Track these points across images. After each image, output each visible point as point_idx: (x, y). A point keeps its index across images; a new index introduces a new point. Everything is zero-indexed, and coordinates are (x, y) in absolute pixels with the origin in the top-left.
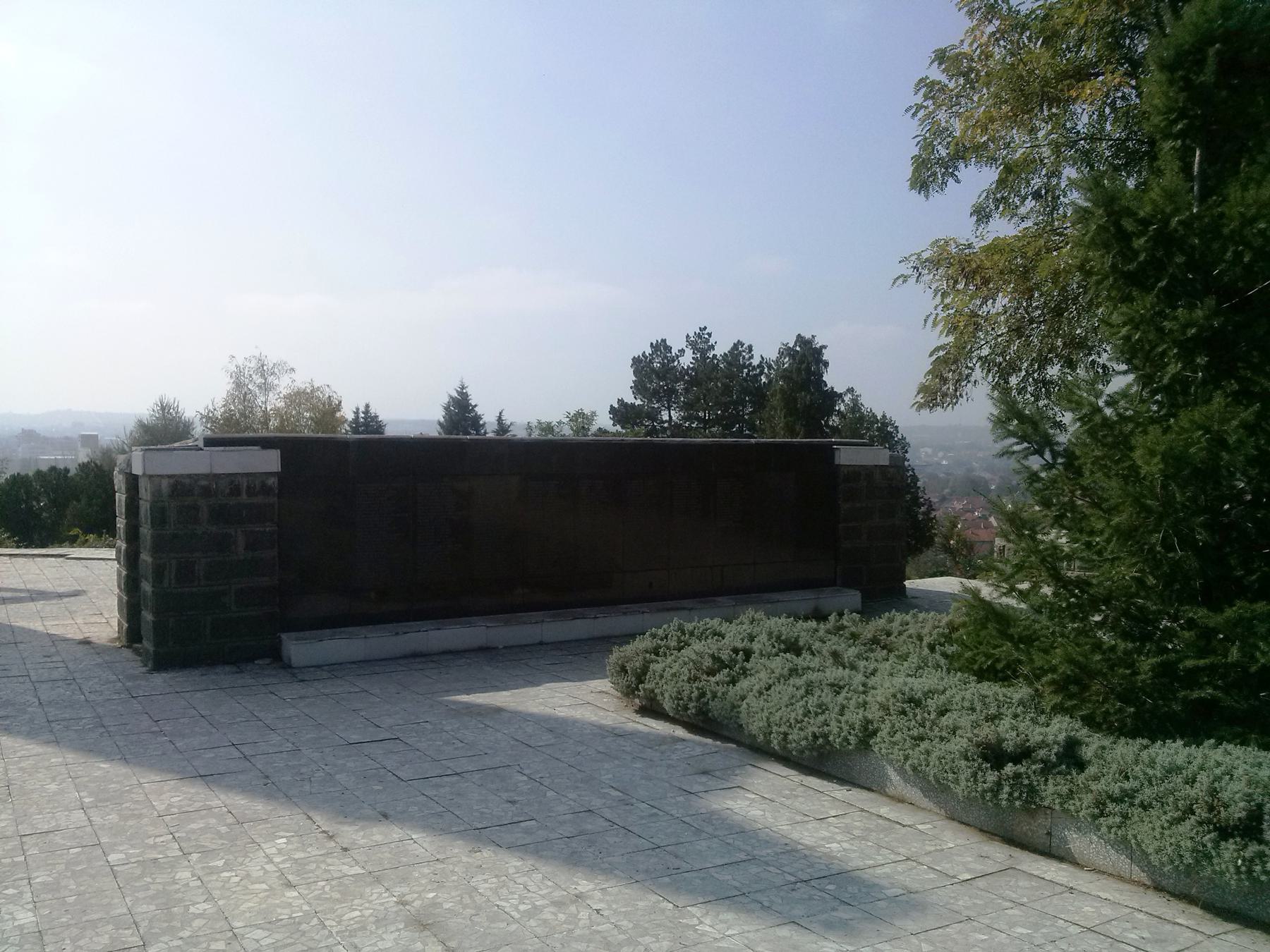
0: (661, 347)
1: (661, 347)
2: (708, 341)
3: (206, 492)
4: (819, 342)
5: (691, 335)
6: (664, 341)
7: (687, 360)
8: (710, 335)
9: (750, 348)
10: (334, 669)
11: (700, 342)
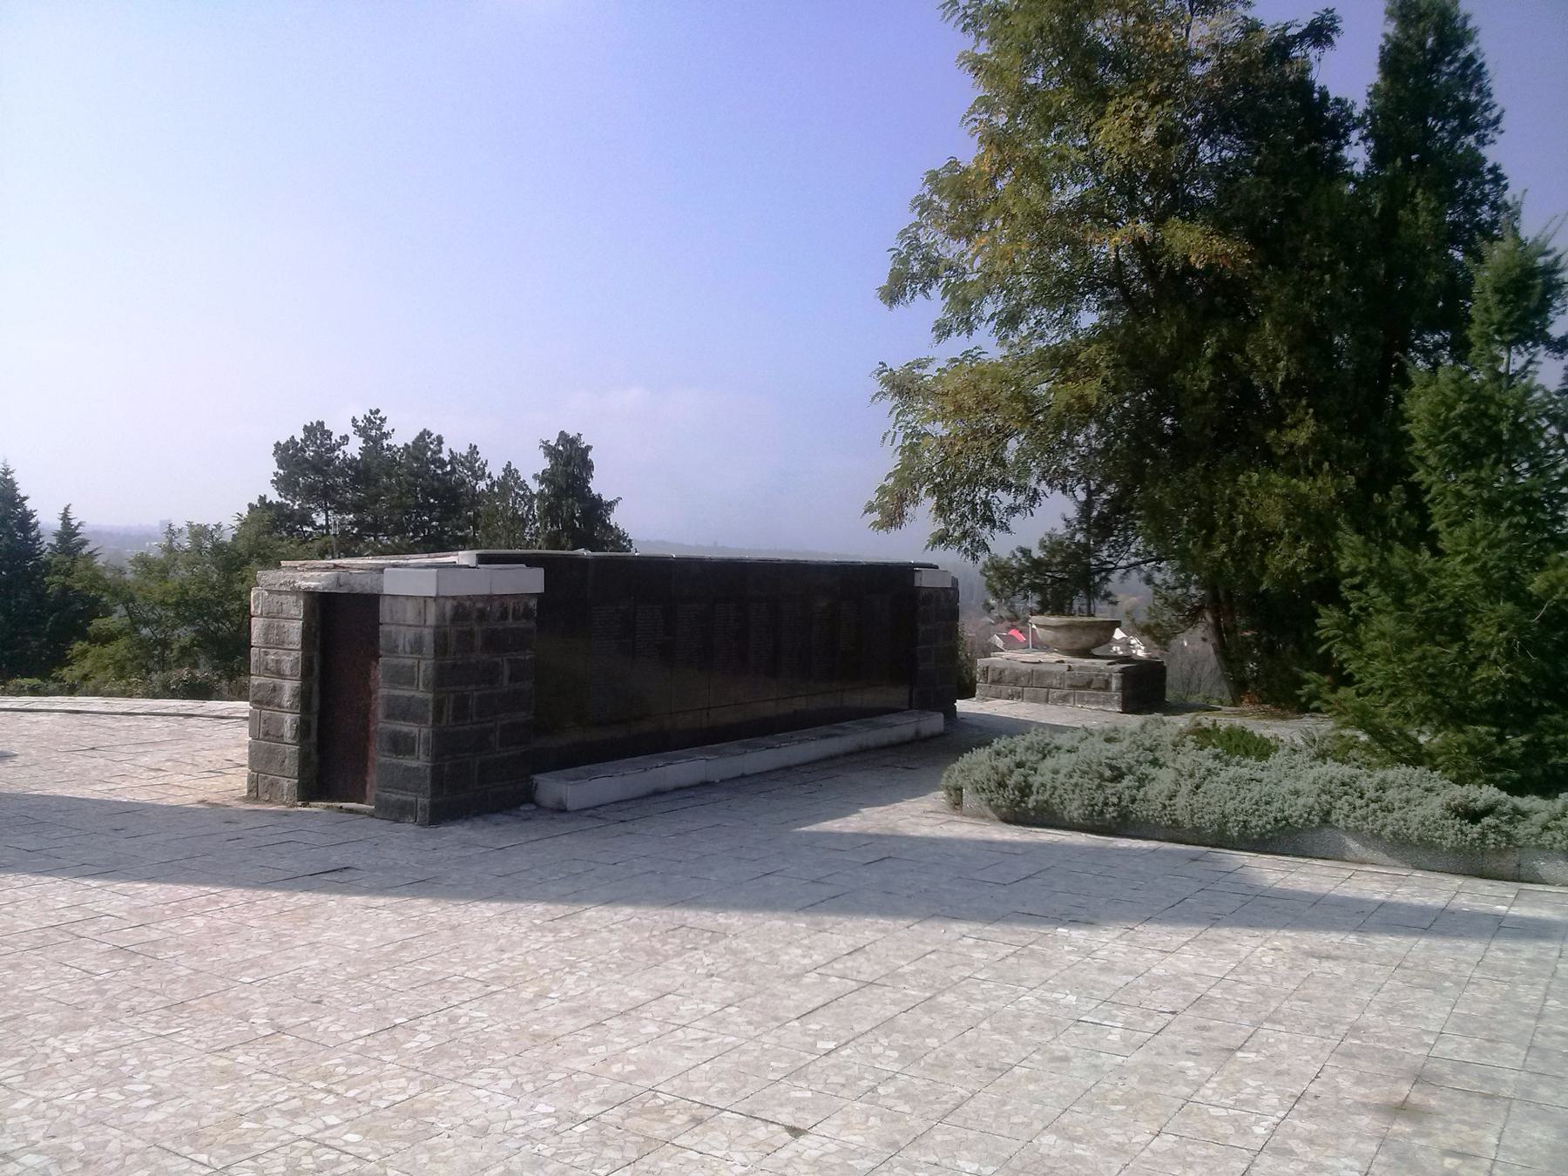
0: (316, 431)
1: (316, 431)
2: (379, 428)
3: (482, 615)
4: (585, 441)
5: (360, 418)
6: (321, 424)
7: (354, 448)
8: (383, 420)
9: (440, 440)
10: (594, 812)
11: (372, 428)
